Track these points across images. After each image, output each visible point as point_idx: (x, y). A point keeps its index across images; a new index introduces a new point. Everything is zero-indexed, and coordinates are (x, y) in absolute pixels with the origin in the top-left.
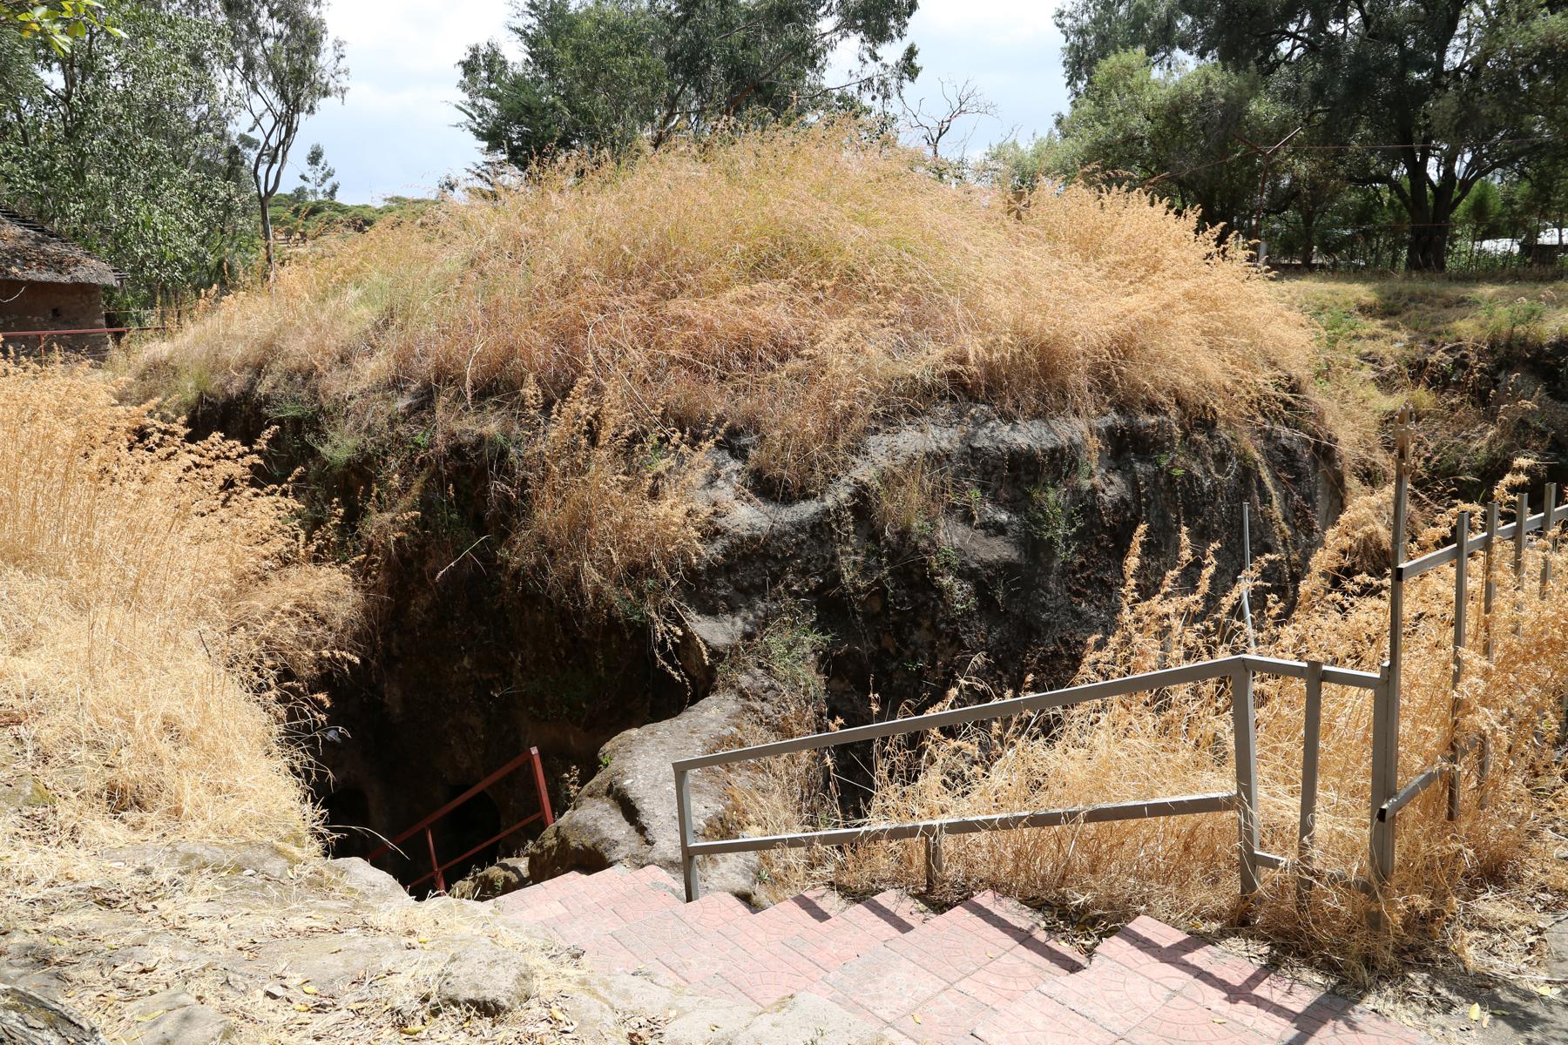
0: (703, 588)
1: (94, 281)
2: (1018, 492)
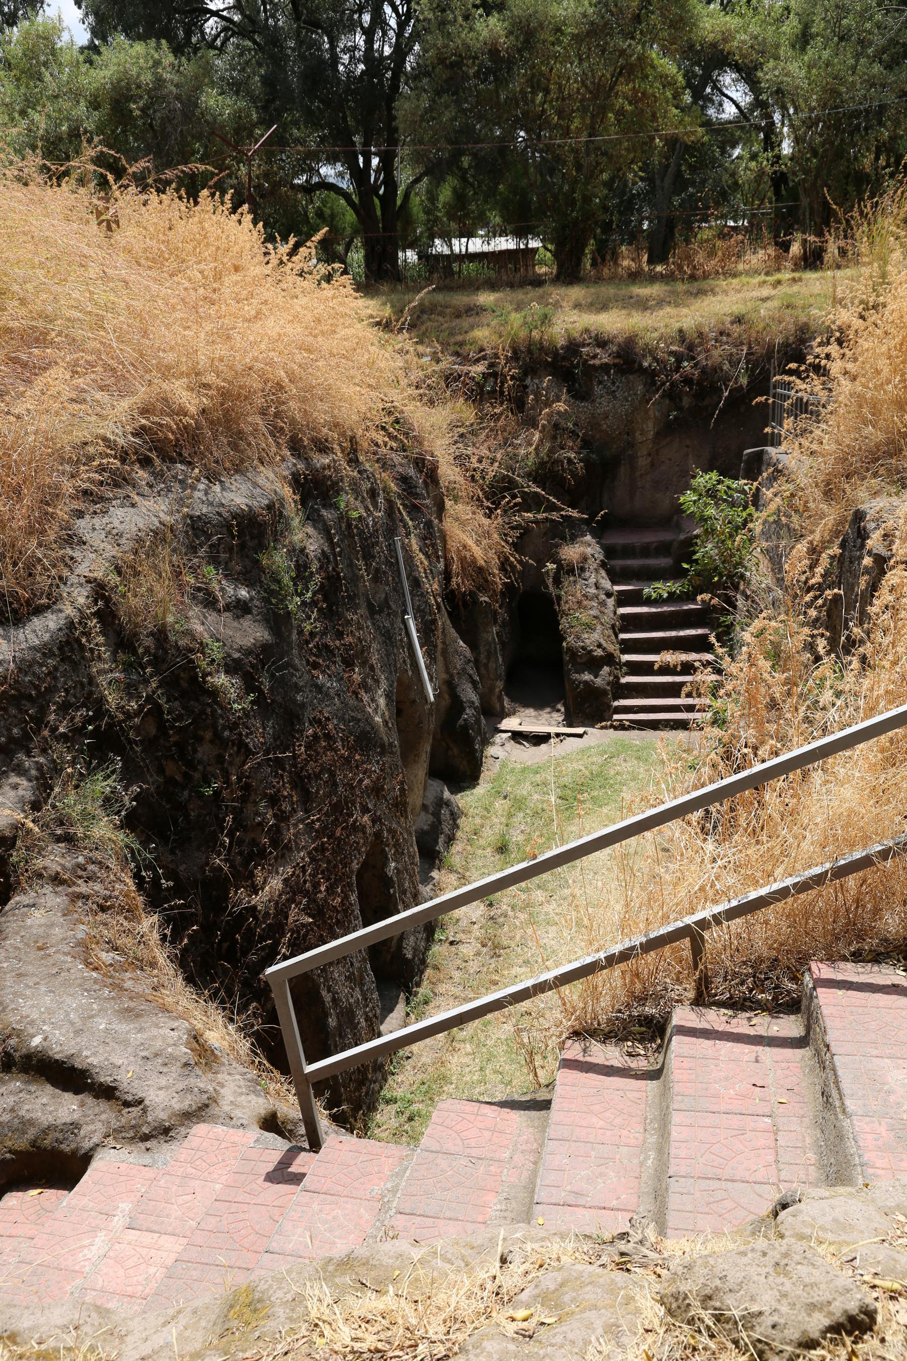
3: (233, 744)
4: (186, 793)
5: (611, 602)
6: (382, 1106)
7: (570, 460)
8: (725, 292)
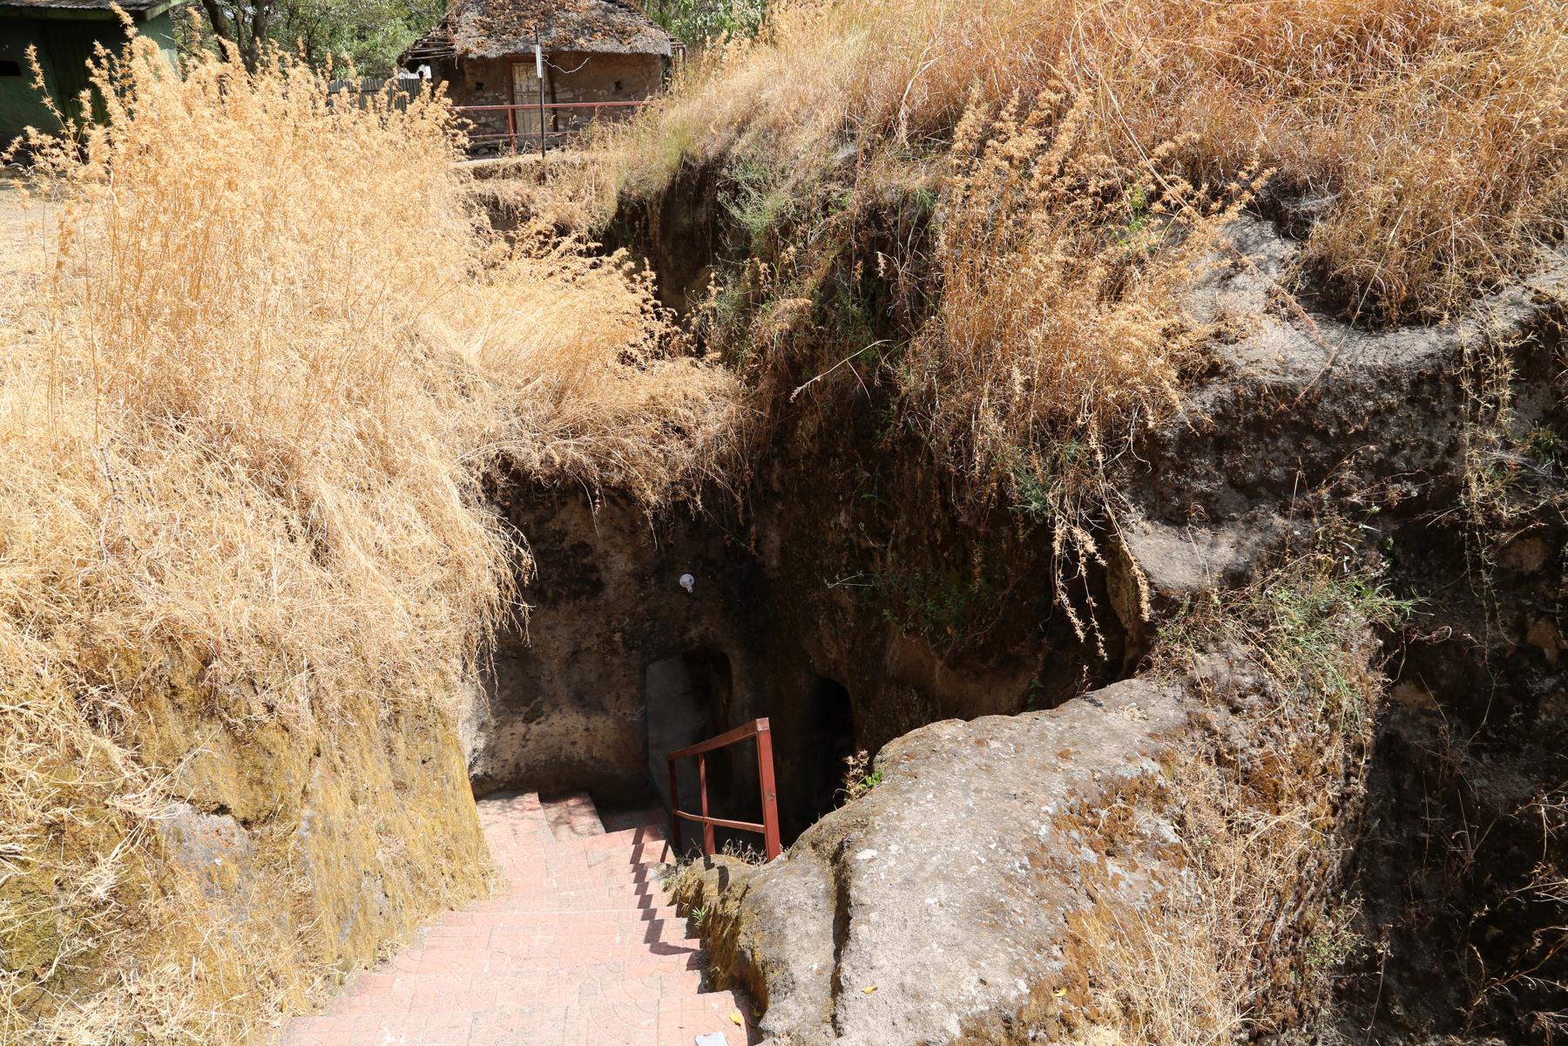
0: (1163, 472)
1: (651, 51)
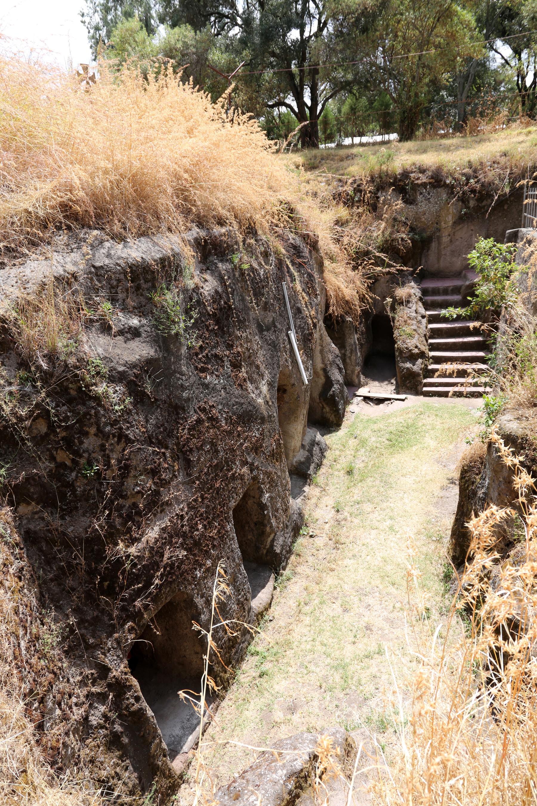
2: (142, 299)
3: (114, 436)
4: (74, 474)
5: (424, 321)
6: (248, 658)
7: (402, 239)
8: (497, 140)
